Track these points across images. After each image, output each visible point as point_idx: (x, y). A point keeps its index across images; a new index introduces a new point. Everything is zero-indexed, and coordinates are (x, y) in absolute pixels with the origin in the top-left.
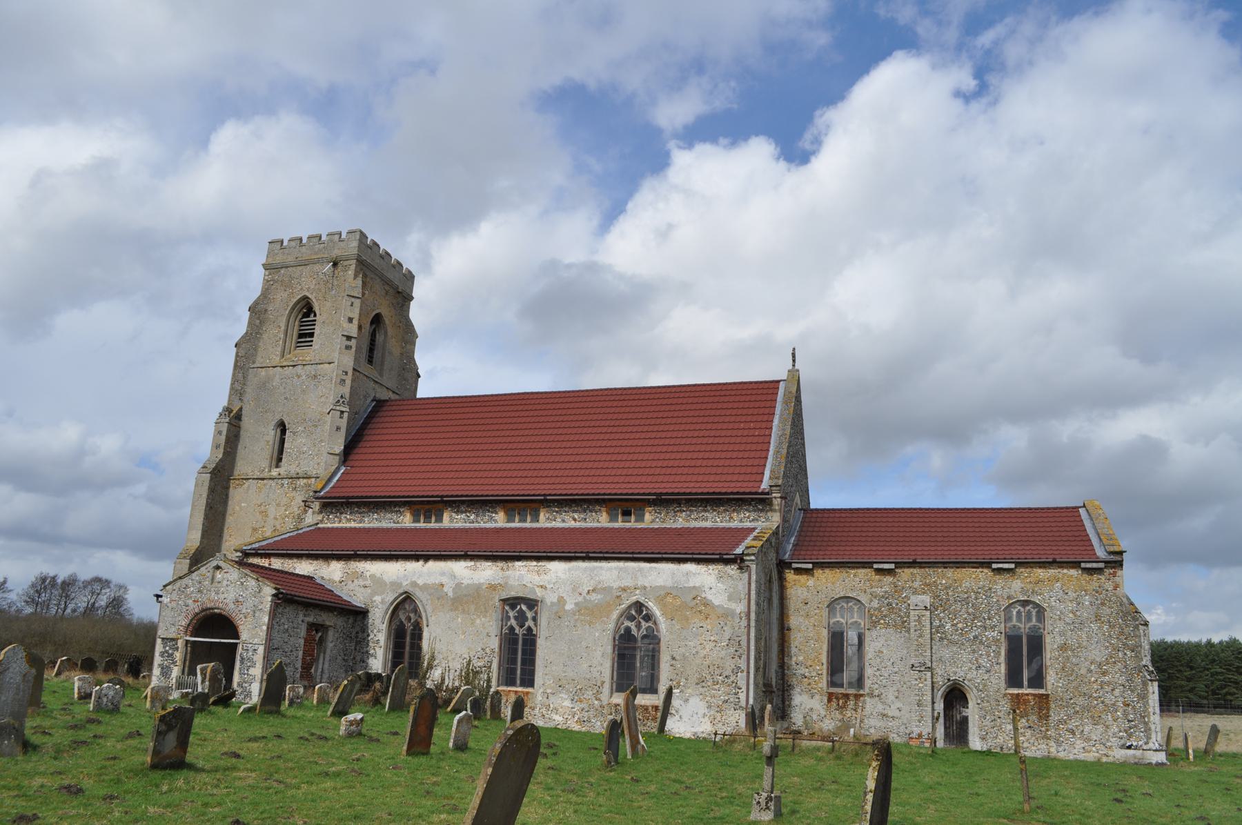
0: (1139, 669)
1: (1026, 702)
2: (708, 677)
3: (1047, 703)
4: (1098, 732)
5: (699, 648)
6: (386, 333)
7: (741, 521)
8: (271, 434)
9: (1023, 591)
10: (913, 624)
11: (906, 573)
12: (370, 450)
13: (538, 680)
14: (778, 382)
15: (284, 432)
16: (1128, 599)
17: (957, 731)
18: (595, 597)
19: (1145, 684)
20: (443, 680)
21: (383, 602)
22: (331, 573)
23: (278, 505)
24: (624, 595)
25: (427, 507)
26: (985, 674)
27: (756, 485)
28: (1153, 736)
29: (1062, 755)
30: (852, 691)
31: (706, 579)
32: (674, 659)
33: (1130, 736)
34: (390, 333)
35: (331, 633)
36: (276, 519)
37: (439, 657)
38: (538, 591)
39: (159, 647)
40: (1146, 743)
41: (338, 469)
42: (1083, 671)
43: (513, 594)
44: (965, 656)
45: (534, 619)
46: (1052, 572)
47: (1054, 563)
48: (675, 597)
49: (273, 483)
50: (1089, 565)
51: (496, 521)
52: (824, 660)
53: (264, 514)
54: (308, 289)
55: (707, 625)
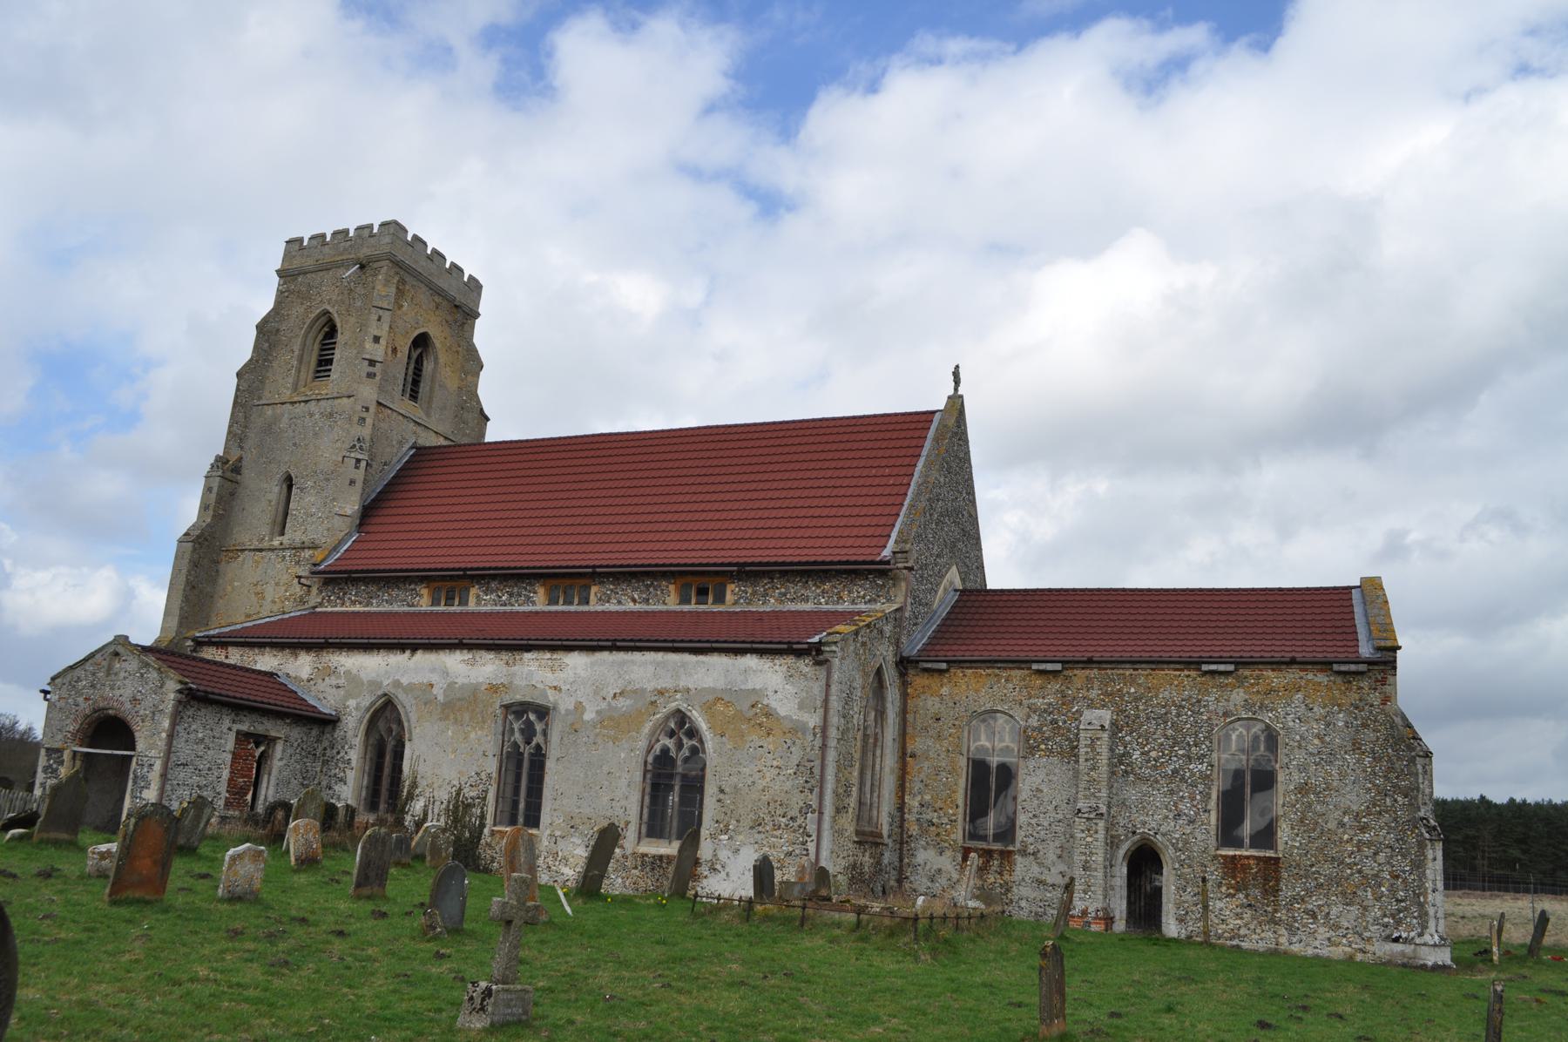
0: (1414, 823)
1: (1245, 868)
2: (767, 819)
3: (1277, 871)
4: (1352, 917)
5: (757, 776)
6: (436, 359)
7: (853, 602)
8: (275, 490)
9: (1247, 705)
10: (1083, 751)
11: (1080, 674)
12: (400, 511)
13: (545, 818)
14: (933, 413)
15: (290, 487)
16: (1404, 718)
17: (1145, 908)
18: (623, 703)
19: (1421, 845)
20: (426, 814)
21: (357, 709)
22: (300, 667)
23: (277, 584)
24: (660, 701)
25: (449, 584)
26: (1185, 827)
27: (876, 551)
28: (1432, 924)
29: (1296, 948)
30: (997, 846)
31: (768, 678)
32: (722, 791)
33: (1399, 923)
34: (441, 361)
35: (279, 747)
36: (273, 602)
37: (422, 783)
38: (550, 693)
39: (42, 761)
40: (1420, 935)
41: (349, 535)
42: (1332, 825)
43: (518, 697)
44: (1159, 798)
45: (545, 733)
46: (1292, 675)
47: (1304, 664)
48: (728, 704)
49: (272, 555)
50: (1344, 668)
51: (534, 603)
52: (960, 802)
53: (260, 595)
54: (329, 301)
55: (769, 743)
